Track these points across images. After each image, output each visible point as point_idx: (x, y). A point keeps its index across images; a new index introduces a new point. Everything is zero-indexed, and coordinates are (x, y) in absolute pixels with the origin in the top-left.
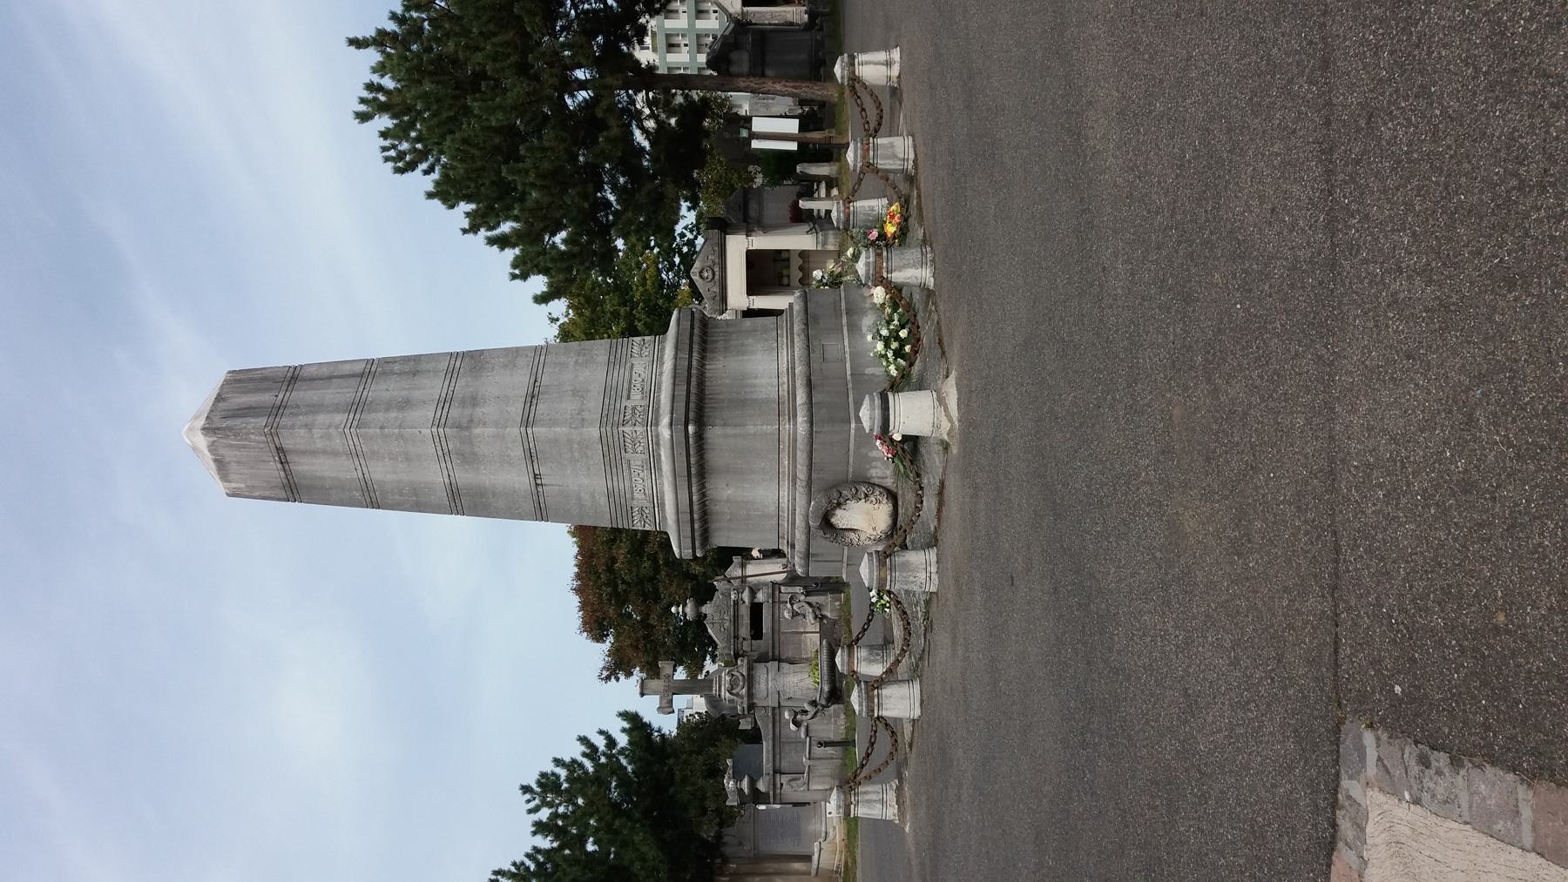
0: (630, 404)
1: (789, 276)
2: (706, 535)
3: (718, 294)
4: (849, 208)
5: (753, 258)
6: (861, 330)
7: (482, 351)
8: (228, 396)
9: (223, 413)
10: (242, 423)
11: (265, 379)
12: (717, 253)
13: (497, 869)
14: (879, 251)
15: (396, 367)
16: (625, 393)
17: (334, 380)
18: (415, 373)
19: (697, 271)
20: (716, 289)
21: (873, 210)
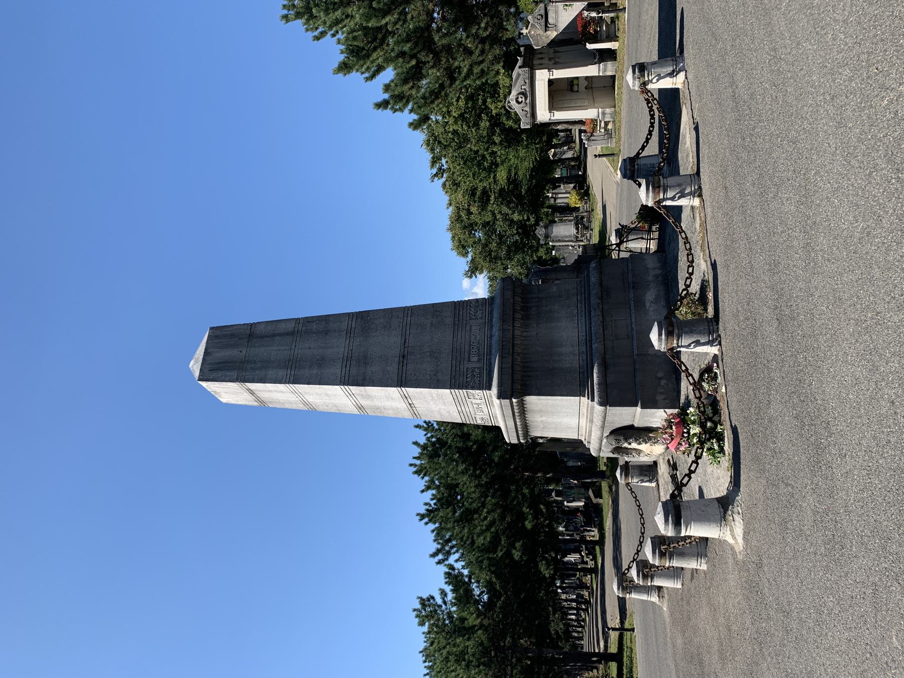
0: (471, 366)
1: (578, 85)
3: (529, 112)
4: (634, 166)
5: (551, 82)
6: (645, 306)
7: (368, 313)
8: (211, 351)
9: (210, 366)
10: (222, 376)
11: (232, 336)
12: (527, 84)
13: (416, 424)
14: (671, 329)
15: (314, 326)
16: (466, 356)
17: (277, 338)
18: (326, 332)
19: (514, 98)
20: (528, 109)
21: (654, 167)
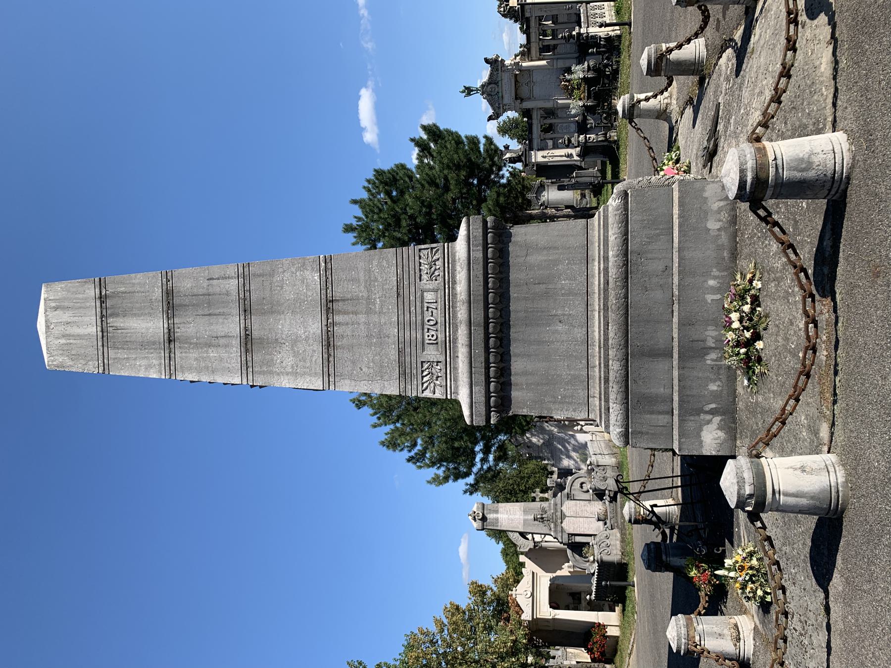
2: (504, 402)
